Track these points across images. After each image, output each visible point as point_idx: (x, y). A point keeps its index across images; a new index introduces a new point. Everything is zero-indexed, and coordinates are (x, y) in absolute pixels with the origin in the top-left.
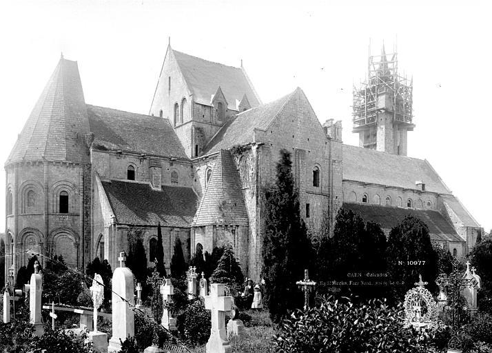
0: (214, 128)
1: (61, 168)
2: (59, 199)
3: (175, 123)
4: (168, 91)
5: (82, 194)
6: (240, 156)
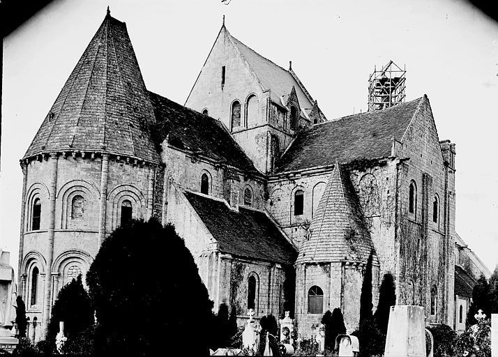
0: (288, 138)
1: (128, 167)
2: (120, 210)
3: (232, 127)
4: (220, 85)
5: (150, 207)
6: (363, 174)
